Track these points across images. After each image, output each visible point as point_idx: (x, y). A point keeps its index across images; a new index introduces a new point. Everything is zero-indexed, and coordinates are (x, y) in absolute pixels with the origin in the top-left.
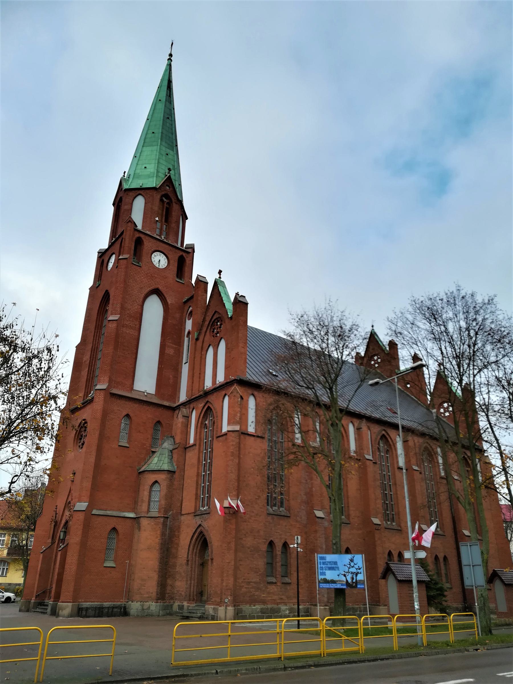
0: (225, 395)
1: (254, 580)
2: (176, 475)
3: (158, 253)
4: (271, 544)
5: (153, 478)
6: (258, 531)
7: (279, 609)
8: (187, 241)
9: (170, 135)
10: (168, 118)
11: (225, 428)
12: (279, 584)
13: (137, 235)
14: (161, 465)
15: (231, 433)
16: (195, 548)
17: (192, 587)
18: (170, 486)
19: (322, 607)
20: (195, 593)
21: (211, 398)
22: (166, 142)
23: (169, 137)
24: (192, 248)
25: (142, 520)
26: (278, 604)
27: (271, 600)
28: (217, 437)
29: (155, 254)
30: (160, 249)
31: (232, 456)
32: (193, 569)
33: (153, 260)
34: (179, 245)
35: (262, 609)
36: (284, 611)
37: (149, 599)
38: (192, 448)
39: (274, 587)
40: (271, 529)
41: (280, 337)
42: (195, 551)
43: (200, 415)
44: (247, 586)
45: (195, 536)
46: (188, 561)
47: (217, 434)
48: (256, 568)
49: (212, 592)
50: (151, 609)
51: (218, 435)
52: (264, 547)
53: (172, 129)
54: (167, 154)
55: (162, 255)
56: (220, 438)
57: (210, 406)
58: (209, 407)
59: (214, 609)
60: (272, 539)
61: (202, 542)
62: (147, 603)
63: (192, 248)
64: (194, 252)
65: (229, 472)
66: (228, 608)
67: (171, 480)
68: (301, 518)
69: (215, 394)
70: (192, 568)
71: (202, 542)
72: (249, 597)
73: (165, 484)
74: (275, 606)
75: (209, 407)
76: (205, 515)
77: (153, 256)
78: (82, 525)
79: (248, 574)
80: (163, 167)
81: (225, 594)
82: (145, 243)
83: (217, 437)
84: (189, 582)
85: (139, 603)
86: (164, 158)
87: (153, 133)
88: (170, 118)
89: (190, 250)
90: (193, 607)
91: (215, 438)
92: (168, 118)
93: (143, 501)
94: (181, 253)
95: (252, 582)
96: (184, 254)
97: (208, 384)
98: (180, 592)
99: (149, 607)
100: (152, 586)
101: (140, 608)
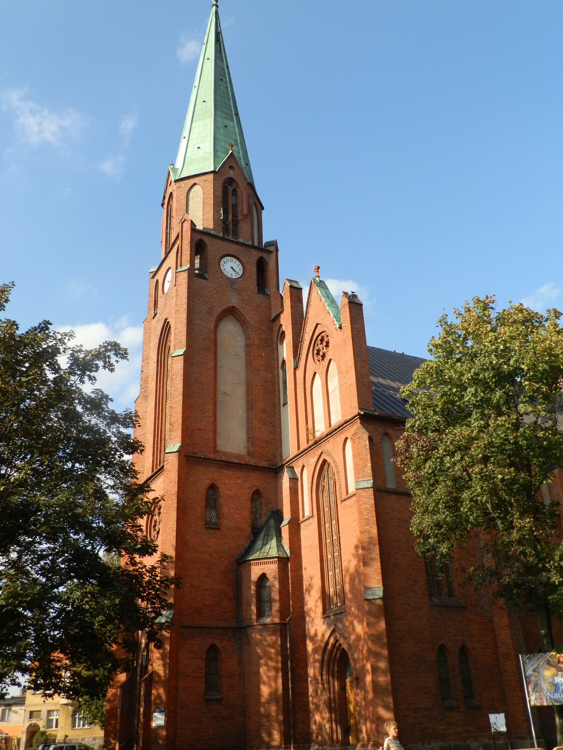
0: (346, 439)
3: (229, 258)
4: (442, 649)
8: (266, 239)
9: (227, 102)
10: (222, 80)
11: (352, 489)
13: (198, 237)
14: (267, 551)
15: (361, 491)
21: (327, 446)
22: (222, 111)
23: (226, 104)
24: (274, 244)
29: (225, 259)
30: (230, 253)
31: (367, 525)
33: (222, 268)
34: (256, 244)
38: (308, 521)
41: (303, 585)
43: (312, 482)
53: (228, 94)
54: (226, 126)
55: (234, 260)
56: (347, 502)
57: (327, 458)
58: (325, 461)
60: (442, 642)
63: (274, 244)
64: (277, 250)
69: (331, 440)
75: (325, 461)
77: (222, 263)
78: (381, 575)
80: (222, 144)
82: (209, 247)
86: (222, 131)
87: (204, 101)
88: (224, 80)
89: (272, 249)
91: (339, 502)
92: (222, 80)
93: (271, 601)
94: (260, 254)
96: (264, 255)
97: (321, 429)
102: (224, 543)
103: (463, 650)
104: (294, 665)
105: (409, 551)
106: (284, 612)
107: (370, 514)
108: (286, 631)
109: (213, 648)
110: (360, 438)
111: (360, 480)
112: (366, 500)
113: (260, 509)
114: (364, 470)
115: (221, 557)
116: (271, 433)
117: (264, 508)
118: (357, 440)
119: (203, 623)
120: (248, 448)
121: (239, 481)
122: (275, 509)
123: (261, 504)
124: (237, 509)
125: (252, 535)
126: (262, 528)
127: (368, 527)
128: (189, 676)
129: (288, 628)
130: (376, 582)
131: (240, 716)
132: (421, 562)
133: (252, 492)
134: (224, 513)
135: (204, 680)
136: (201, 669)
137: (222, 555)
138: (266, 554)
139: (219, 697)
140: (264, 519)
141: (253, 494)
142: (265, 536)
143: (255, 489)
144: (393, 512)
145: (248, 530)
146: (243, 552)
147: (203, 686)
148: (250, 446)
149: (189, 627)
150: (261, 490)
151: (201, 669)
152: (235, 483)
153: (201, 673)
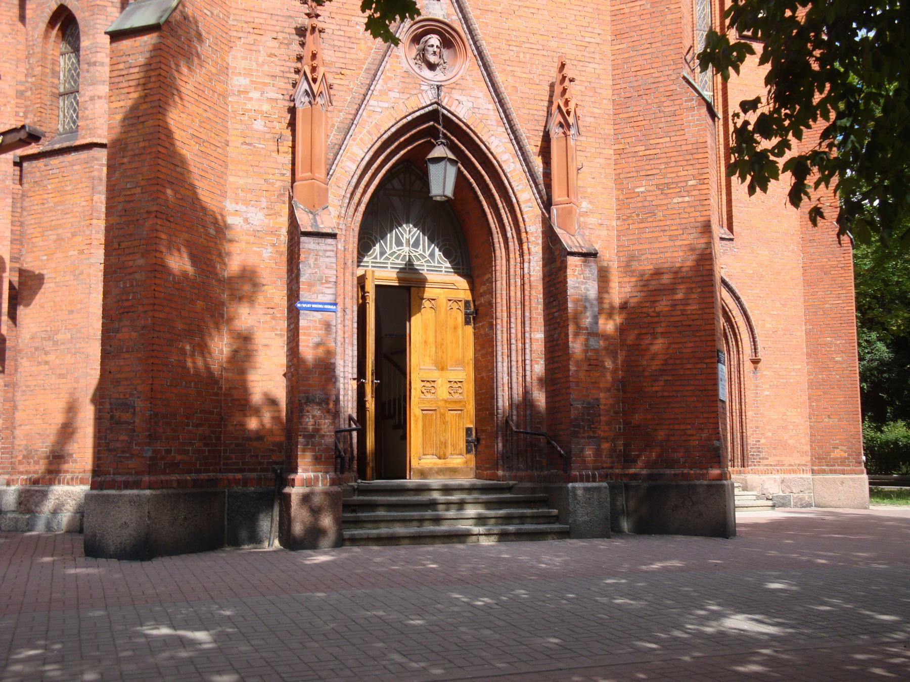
49: (763, 441)
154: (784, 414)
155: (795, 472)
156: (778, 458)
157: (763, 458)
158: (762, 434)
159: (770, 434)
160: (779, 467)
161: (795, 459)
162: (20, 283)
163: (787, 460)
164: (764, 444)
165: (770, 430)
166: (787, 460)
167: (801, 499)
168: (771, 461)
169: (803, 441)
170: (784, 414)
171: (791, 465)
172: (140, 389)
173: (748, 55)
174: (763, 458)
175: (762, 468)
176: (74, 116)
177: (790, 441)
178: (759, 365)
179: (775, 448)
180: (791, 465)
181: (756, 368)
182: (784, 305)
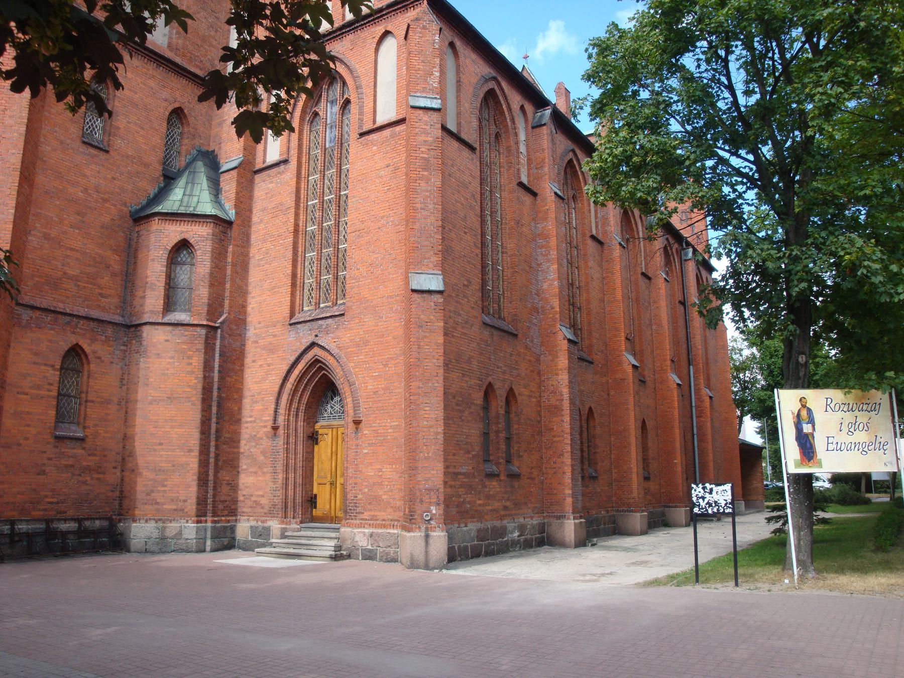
0: (387, 33)
1: (464, 470)
2: (234, 232)
5: (173, 232)
6: (469, 361)
7: (504, 528)
12: (502, 477)
14: (194, 205)
16: (297, 399)
17: (290, 487)
18: (219, 256)
19: (577, 521)
20: (299, 500)
25: (146, 330)
26: (501, 518)
27: (491, 510)
28: (362, 135)
31: (425, 169)
32: (292, 446)
35: (479, 531)
36: (512, 532)
37: (180, 513)
39: (495, 483)
40: (489, 359)
42: (295, 405)
44: (453, 483)
45: (296, 372)
46: (275, 428)
47: (360, 127)
48: (467, 444)
49: (360, 496)
50: (185, 536)
51: (365, 129)
52: (478, 398)
59: (371, 535)
60: (490, 379)
61: (318, 386)
62: (174, 525)
65: (419, 206)
66: (432, 534)
67: (221, 240)
68: (532, 341)
70: (288, 443)
71: (318, 386)
72: (457, 506)
73: (209, 249)
74: (498, 523)
76: (330, 321)
79: (454, 455)
81: (421, 501)
83: (362, 135)
84: (281, 476)
85: (152, 524)
90: (294, 530)
95: (461, 474)
98: (253, 499)
99: (180, 533)
100: (184, 486)
101: (156, 534)
102: (114, 178)
103: (511, 395)
104: (223, 395)
105: (465, 233)
106: (214, 307)
107: (432, 153)
108: (216, 339)
109: (76, 352)
110: (424, 28)
111: (418, 94)
112: (428, 127)
113: (180, 142)
114: (426, 80)
115: (105, 201)
116: (212, 26)
117: (186, 141)
118: (419, 29)
119: (61, 305)
120: (170, 38)
121: (152, 83)
122: (204, 149)
123: (181, 134)
124: (143, 128)
125: (162, 178)
126: (180, 173)
127: (426, 173)
128: (27, 394)
129: (219, 336)
130: (431, 265)
131: (115, 468)
132: (477, 255)
133: (170, 108)
134: (119, 128)
135: (55, 403)
136: (51, 384)
137: (106, 196)
138: (192, 209)
139: (80, 435)
140: (183, 161)
141: (171, 114)
142: (187, 183)
143: (177, 105)
144: (452, 165)
145: (157, 170)
146: (144, 202)
147: (53, 413)
148: (174, 36)
149: (33, 308)
150: (185, 111)
151: (51, 384)
152: (144, 84)
153: (49, 390)
154: (380, 470)
155: (385, 527)
156: (372, 513)
157: (359, 513)
158: (360, 490)
159: (366, 490)
160: (373, 521)
161: (387, 514)
162: (575, 334)
163: (381, 515)
164: (361, 500)
165: (366, 486)
166: (381, 515)
167: (387, 554)
168: (366, 515)
169: (397, 496)
170: (380, 470)
171: (384, 520)
172: (509, 350)
173: (741, 437)
174: (359, 513)
175: (358, 522)
176: (238, 281)
177: (384, 497)
178: (361, 425)
179: (370, 504)
180: (384, 520)
181: (357, 429)
182: (385, 365)
